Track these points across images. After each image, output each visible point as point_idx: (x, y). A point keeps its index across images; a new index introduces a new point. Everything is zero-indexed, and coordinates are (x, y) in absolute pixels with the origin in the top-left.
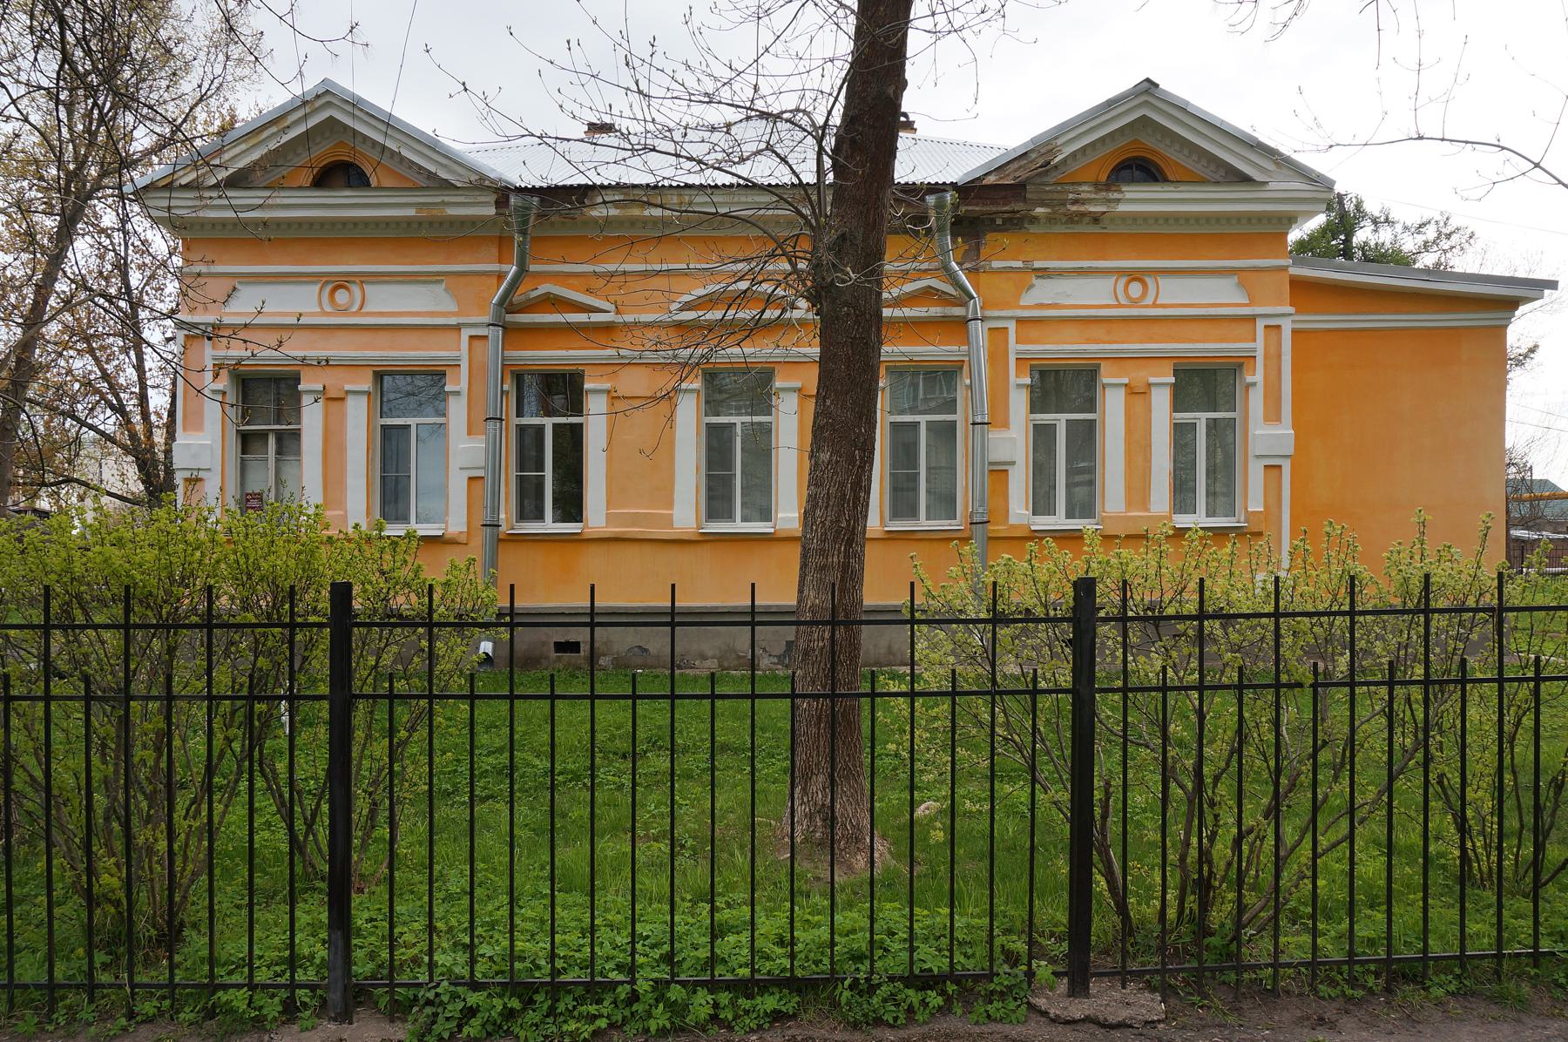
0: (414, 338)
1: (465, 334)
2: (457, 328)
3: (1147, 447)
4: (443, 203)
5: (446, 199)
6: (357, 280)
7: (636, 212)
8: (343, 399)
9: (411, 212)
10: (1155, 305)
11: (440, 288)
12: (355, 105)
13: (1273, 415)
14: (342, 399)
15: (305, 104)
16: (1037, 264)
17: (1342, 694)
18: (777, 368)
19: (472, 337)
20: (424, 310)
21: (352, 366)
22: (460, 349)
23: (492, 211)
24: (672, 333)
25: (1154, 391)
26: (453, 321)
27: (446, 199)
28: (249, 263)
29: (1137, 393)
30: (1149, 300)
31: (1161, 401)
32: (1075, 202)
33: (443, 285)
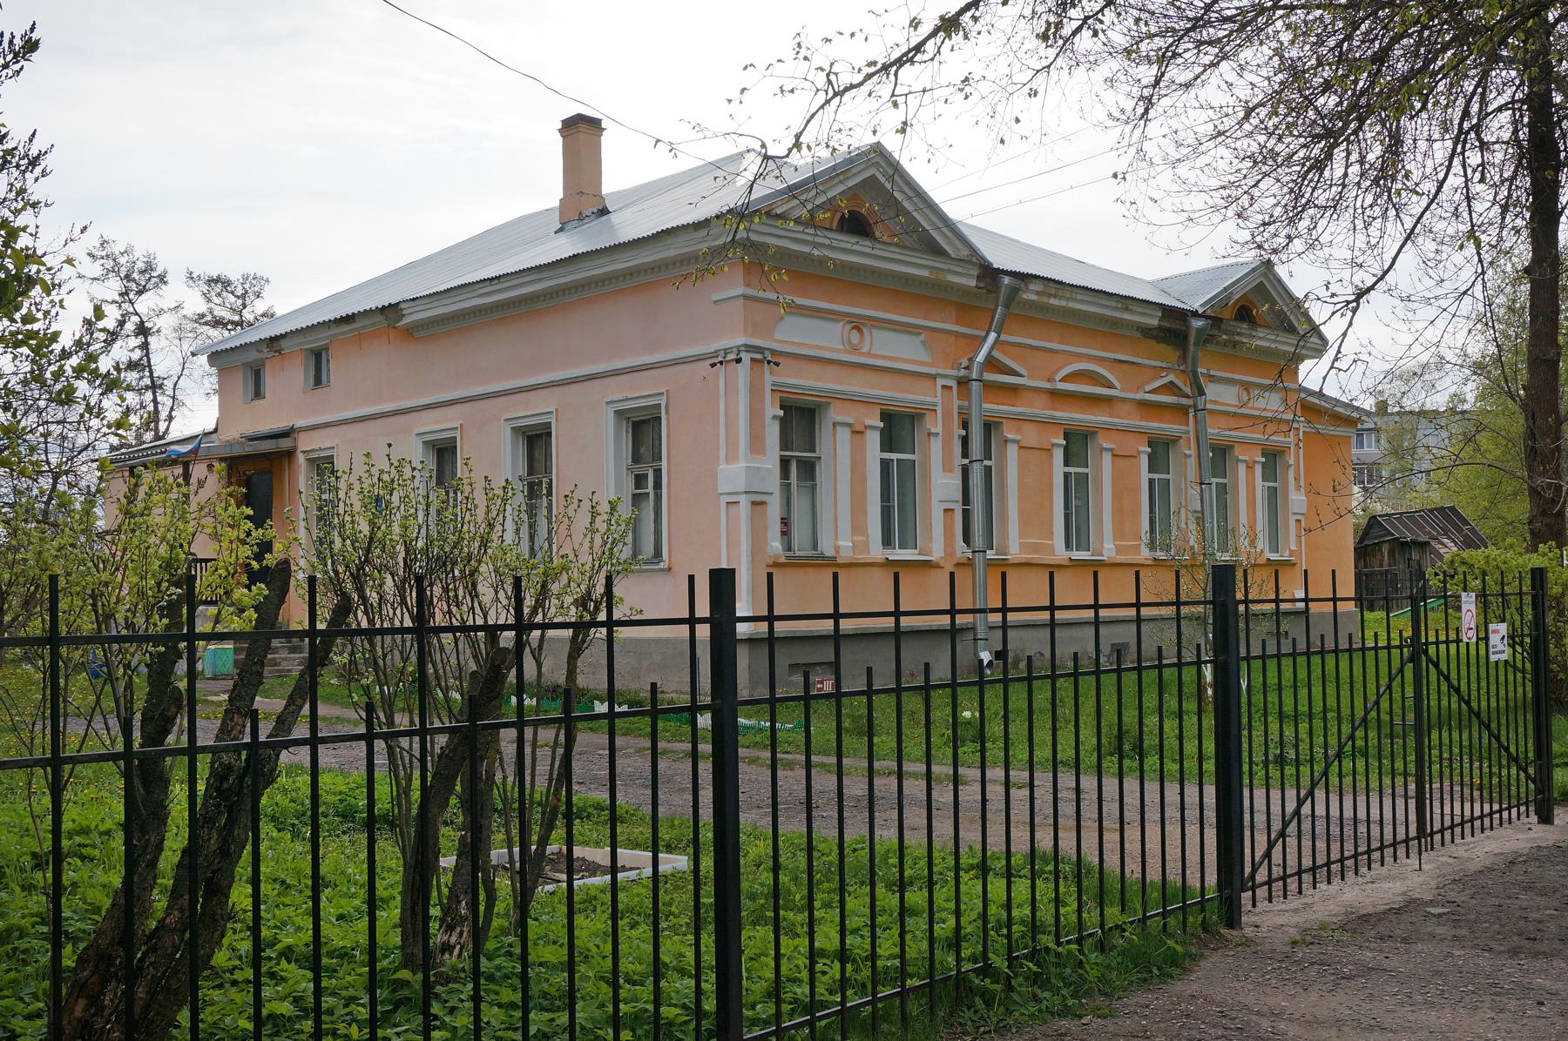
0: (832, 370)
1: (940, 382)
2: (934, 377)
3: (863, 480)
4: (949, 271)
5: (952, 268)
6: (869, 323)
7: (1045, 299)
8: (862, 433)
9: (925, 273)
10: (869, 354)
11: (917, 340)
12: (896, 169)
13: (1298, 487)
14: (862, 433)
15: (853, 161)
16: (1212, 373)
17: (1430, 640)
18: (1236, 445)
19: (944, 387)
20: (910, 357)
21: (866, 402)
22: (938, 398)
23: (973, 283)
24: (380, 318)
25: (868, 431)
26: (933, 371)
27: (952, 268)
28: (831, 301)
29: (1250, 467)
30: (1250, 405)
31: (873, 440)
32: (1239, 334)
33: (922, 337)
